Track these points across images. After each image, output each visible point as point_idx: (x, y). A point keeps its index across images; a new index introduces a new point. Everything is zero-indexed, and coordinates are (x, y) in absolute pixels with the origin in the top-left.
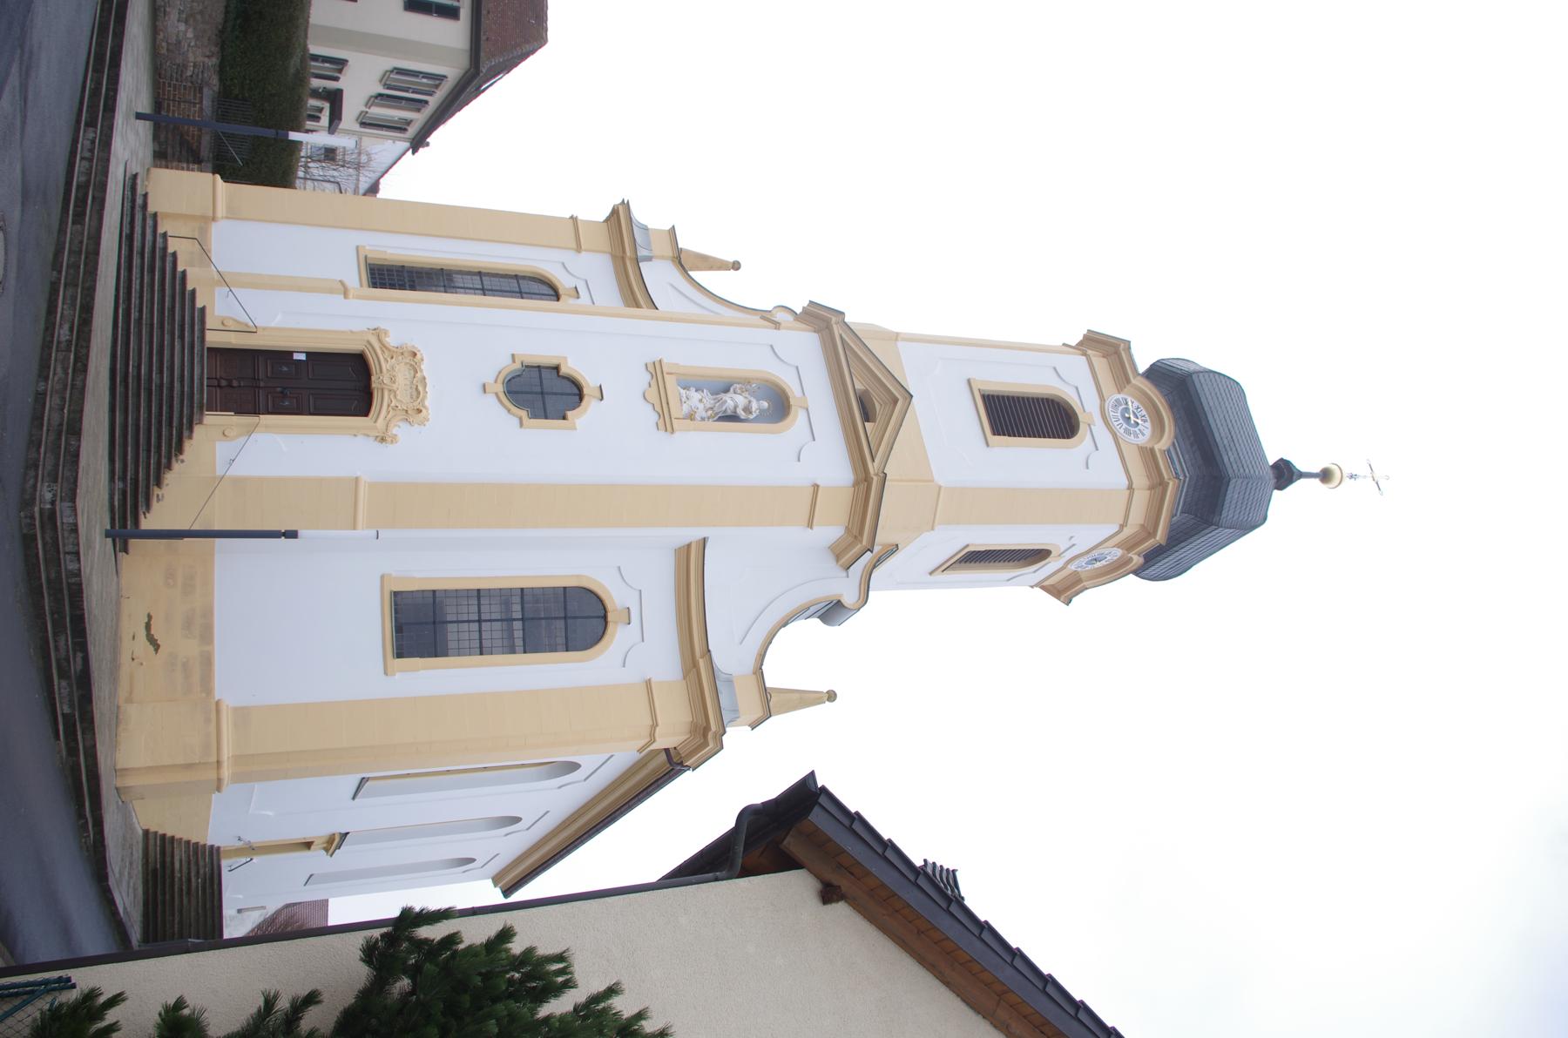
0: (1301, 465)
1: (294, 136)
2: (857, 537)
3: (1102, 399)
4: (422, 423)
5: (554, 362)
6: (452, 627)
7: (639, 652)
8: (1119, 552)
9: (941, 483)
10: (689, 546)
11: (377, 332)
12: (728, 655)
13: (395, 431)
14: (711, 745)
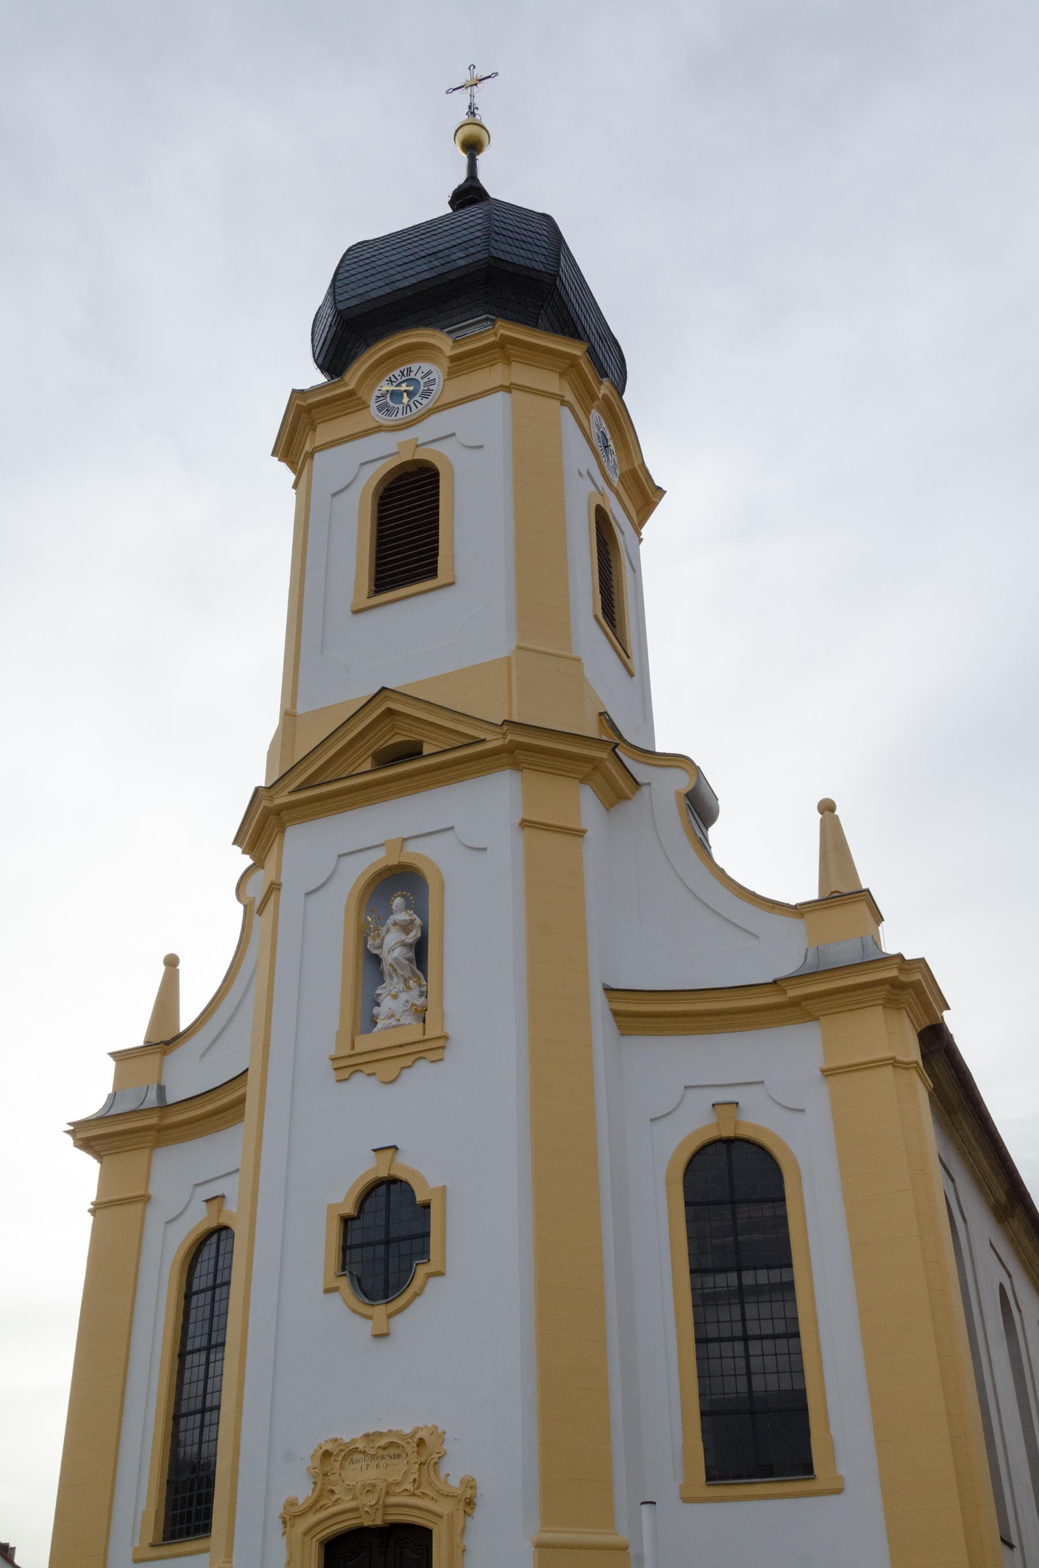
0: (460, 177)
2: (595, 765)
3: (378, 429)
4: (441, 1437)
5: (336, 1225)
7: (785, 1090)
8: (595, 414)
9: (513, 646)
10: (616, 1014)
12: (781, 956)
13: (454, 1482)
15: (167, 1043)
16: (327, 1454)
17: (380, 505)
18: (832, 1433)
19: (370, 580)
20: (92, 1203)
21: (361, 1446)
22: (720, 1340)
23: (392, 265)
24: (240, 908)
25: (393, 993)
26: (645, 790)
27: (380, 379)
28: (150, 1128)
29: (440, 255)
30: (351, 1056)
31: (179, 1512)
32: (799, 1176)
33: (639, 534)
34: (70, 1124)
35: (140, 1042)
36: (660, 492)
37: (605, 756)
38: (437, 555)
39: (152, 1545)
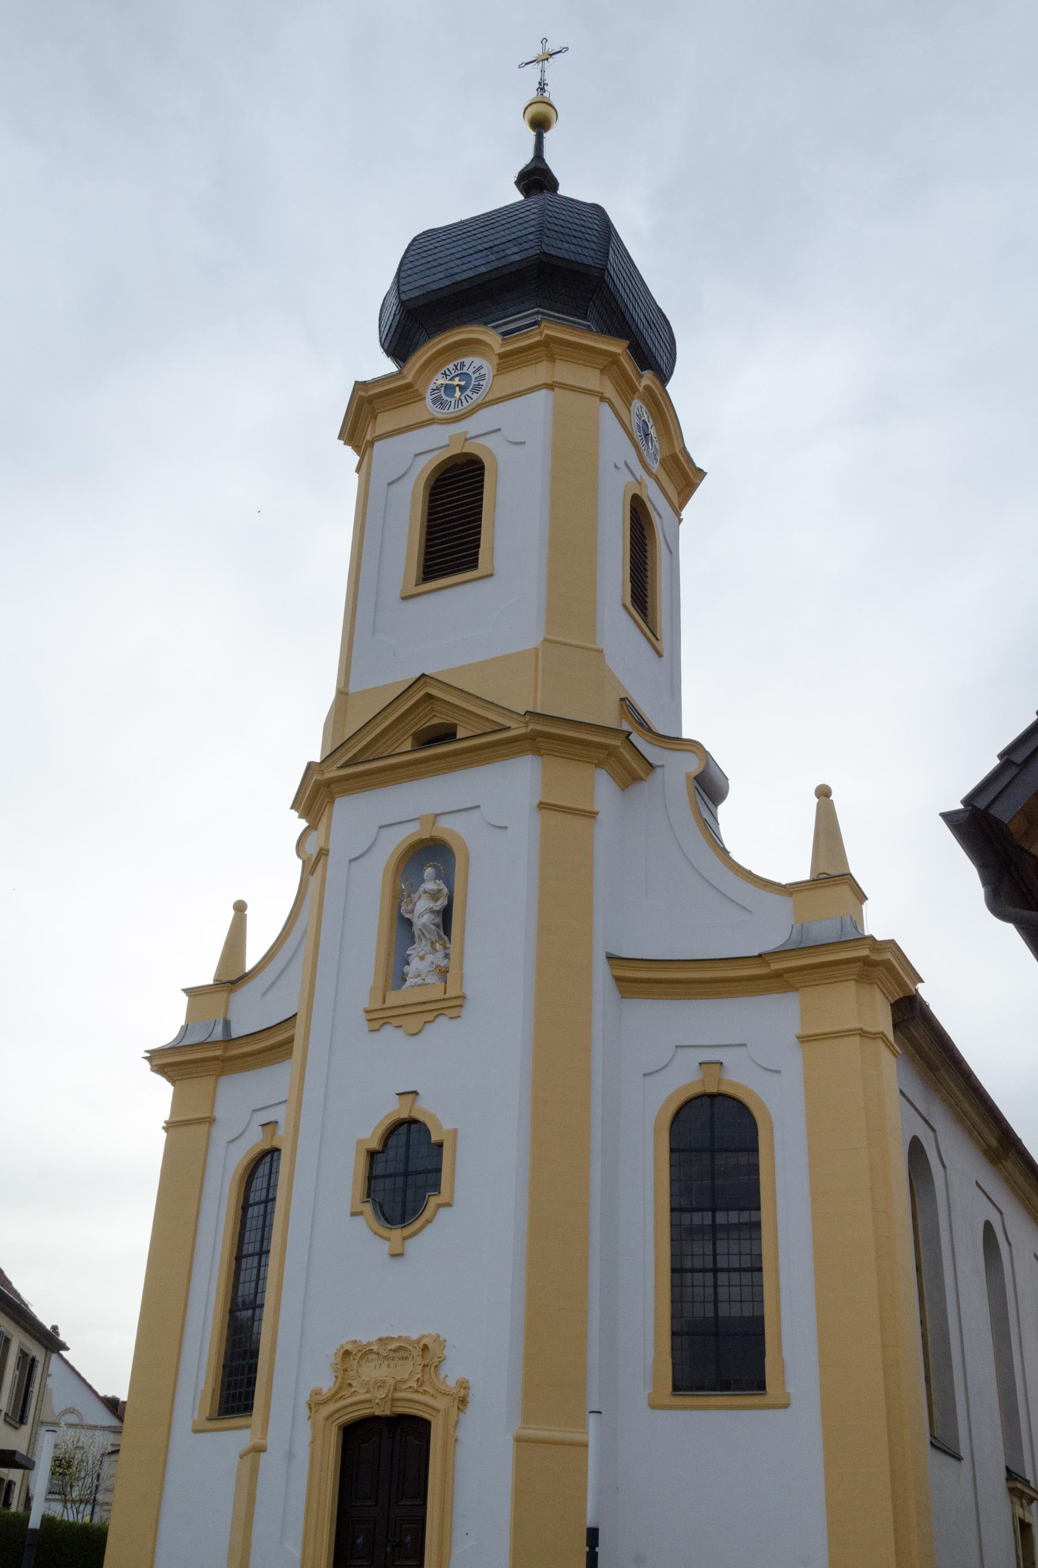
0: (526, 157)
1: (35, 1522)
2: (611, 752)
3: (432, 421)
4: (442, 1344)
5: (363, 1158)
6: (724, 1311)
8: (637, 404)
9: (541, 638)
10: (617, 979)
11: (314, 1405)
12: (767, 933)
13: (451, 1383)
14: (888, 956)
15: (233, 983)
16: (347, 1353)
17: (431, 495)
18: (784, 1356)
19: (418, 567)
20: (166, 1122)
21: (375, 1348)
22: (693, 1271)
23: (453, 257)
24: (300, 862)
25: (420, 954)
26: (659, 770)
27: (436, 372)
28: (215, 1058)
29: (496, 249)
30: (382, 1009)
31: (232, 1392)
32: (772, 1129)
33: (678, 515)
34: (147, 1051)
35: (210, 981)
36: (701, 474)
37: (618, 743)
38: (478, 546)
39: (209, 1419)
